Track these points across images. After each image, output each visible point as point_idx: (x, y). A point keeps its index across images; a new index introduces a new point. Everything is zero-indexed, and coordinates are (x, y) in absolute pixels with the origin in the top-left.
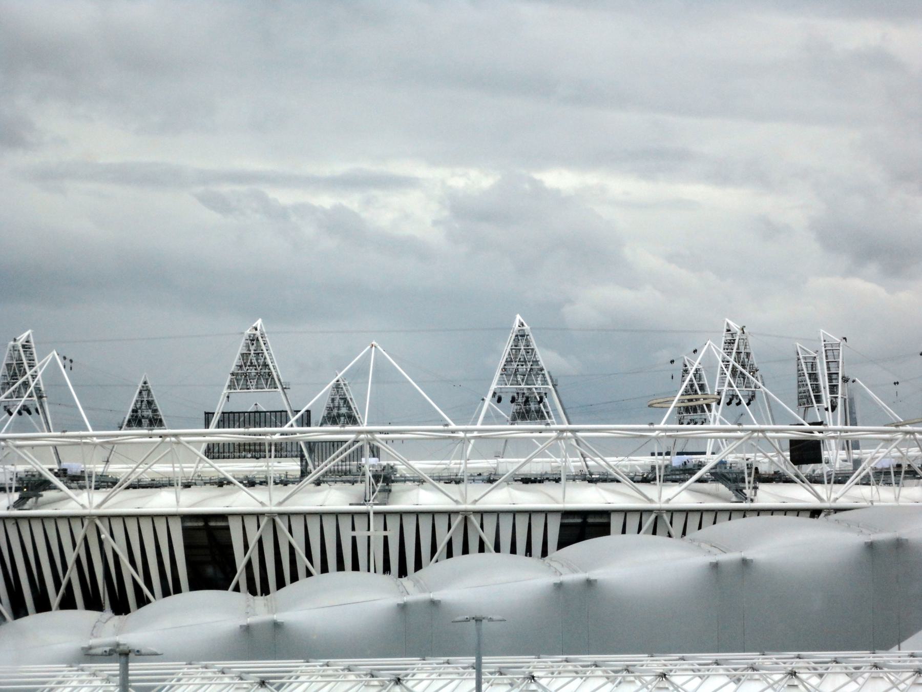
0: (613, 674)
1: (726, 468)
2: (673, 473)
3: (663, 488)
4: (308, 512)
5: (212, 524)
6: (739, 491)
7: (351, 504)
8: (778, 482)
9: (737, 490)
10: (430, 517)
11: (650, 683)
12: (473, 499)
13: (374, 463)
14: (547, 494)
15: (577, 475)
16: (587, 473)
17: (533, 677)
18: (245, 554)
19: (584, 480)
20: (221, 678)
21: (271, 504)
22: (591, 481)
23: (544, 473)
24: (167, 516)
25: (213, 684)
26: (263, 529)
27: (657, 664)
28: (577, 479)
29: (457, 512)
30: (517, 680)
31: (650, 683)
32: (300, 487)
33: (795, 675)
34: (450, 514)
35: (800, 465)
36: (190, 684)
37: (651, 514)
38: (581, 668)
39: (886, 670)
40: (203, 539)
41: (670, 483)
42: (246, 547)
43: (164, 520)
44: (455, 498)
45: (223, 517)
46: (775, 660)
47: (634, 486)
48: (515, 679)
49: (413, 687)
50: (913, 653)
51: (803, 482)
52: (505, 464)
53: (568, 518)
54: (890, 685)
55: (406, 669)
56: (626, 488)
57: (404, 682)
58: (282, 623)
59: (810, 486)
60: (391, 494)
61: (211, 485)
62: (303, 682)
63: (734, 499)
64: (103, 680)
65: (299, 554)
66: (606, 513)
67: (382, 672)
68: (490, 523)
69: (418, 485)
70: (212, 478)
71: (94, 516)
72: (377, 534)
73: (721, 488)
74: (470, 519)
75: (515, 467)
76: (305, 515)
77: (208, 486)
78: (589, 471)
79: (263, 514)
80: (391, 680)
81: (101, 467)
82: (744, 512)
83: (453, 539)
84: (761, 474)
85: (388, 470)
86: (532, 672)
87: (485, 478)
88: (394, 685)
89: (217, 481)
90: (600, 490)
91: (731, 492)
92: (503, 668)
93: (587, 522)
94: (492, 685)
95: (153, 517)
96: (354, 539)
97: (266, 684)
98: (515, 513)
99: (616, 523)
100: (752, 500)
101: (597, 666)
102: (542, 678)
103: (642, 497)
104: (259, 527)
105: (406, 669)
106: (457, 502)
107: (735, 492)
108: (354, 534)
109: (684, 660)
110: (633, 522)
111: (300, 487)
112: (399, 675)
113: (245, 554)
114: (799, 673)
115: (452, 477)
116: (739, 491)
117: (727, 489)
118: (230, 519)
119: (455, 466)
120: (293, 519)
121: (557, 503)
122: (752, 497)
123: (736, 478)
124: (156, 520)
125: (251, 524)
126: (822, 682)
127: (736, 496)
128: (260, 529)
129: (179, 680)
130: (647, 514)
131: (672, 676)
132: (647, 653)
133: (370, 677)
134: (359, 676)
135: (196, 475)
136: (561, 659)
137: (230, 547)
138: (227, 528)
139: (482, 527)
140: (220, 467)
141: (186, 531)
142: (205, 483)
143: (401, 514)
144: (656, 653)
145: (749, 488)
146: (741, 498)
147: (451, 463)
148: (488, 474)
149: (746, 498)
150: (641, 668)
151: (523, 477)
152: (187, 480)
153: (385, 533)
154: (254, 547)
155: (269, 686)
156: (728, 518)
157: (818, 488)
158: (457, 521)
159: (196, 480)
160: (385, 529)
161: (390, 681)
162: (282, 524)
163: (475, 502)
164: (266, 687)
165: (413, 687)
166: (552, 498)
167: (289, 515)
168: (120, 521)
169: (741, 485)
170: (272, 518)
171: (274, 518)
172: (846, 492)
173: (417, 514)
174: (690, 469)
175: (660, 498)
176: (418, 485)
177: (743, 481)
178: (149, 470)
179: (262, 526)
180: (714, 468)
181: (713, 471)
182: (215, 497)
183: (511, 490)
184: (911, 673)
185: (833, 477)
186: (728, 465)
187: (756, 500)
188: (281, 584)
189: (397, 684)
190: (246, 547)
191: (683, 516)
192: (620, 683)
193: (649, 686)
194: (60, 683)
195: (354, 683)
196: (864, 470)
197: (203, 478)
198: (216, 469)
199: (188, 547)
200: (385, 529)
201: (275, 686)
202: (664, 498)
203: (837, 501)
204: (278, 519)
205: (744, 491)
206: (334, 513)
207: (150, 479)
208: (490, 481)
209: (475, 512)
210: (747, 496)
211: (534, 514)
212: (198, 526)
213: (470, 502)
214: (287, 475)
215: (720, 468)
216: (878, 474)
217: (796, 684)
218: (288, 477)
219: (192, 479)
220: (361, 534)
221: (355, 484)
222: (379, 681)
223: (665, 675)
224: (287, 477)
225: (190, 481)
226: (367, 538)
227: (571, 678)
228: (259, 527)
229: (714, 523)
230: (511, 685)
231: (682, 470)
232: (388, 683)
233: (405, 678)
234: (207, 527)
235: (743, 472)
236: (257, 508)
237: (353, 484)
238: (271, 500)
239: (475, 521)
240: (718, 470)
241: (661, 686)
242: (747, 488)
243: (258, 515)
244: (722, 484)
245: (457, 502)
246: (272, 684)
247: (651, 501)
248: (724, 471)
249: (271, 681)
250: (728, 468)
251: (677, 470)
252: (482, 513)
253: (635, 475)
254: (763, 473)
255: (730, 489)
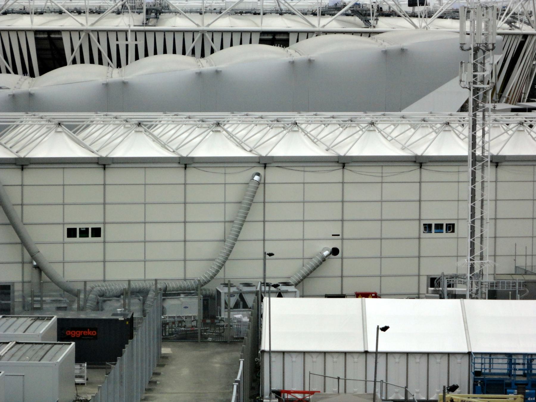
0: (271, 122)
1: (359, 7)
2: (330, 10)
3: (321, 18)
4: (156, 30)
5: (53, 36)
6: (367, 21)
7: (135, 26)
8: (393, 16)
9: (366, 21)
10: (106, 33)
11: (364, 128)
12: (207, 24)
13: (149, 1)
14: (254, 22)
15: (273, 10)
16: (279, 9)
17: (296, 123)
18: (72, 54)
19: (277, 13)
20: (188, 121)
21: (87, 25)
22: (281, 14)
23: (253, 9)
24: (25, 31)
25: (36, 124)
26: (83, 39)
27: (369, 117)
28: (273, 13)
29: (197, 31)
30: (287, 125)
31: (364, 128)
32: (104, 15)
33: (373, 124)
34: (193, 32)
35: (414, 7)
36: (98, 124)
37: (314, 34)
38: (254, 119)
39: (502, 122)
40: (46, 45)
41: (329, 15)
42: (73, 50)
43: (24, 33)
44: (197, 23)
45: (58, 32)
46: (239, 116)
47: (303, 17)
48: (286, 125)
49: (228, 128)
50: (333, 115)
51: (406, 17)
52: (252, 4)
53: (264, 36)
54: (503, 131)
55: (224, 118)
56: (299, 18)
57: (223, 125)
58: (34, 93)
59: (410, 19)
60: (159, 20)
61: (55, 13)
62: (163, 124)
63: (364, 26)
64: (47, 121)
65: (104, 55)
66: (287, 33)
67: (209, 119)
68: (121, 36)
69: (176, 15)
70: (56, 9)
71: (89, 30)
72: (131, 42)
73: (356, 19)
74: (205, 35)
75: (233, 5)
76: (107, 32)
77: (53, 13)
78: (280, 8)
79: (82, 31)
80: (214, 124)
81: (44, 2)
82: (370, 34)
83: (195, 48)
84: (384, 12)
85: (158, 5)
86: (295, 121)
87: (218, 11)
88: (216, 126)
89: (58, 11)
90: (284, 19)
91: (362, 22)
92: (353, 118)
93: (275, 38)
94: (272, 128)
95: (17, 31)
96: (118, 46)
97: (141, 125)
98: (232, 32)
99: (292, 38)
100: (374, 27)
101: (190, 118)
102: (302, 124)
103: (309, 24)
104: (80, 38)
105: (224, 118)
106: (198, 25)
107: (365, 22)
108: (117, 43)
109: (177, 116)
110: (246, 37)
111: (104, 15)
112: (219, 121)
113: (72, 54)
114: (451, 123)
115: (198, 11)
116: (367, 21)
117: (360, 20)
118: (63, 33)
119: (215, 4)
120: (215, 35)
121: (258, 26)
122: (375, 25)
123: (366, 14)
124: (72, 33)
125: (75, 36)
126: (464, 130)
127: (365, 24)
128: (81, 39)
129: (22, 122)
130: (311, 34)
131: (378, 124)
132: (94, 112)
133: (126, 122)
134: (195, 121)
135: (46, 7)
136: (244, 114)
137: (63, 50)
138: (61, 39)
139: (213, 40)
140: (58, 3)
141: (37, 39)
142: (51, 12)
143: (164, 32)
144: (368, 111)
145: (373, 19)
146: (368, 26)
147: (212, 3)
148: (219, 9)
149: (371, 26)
150: (360, 119)
151: (240, 11)
152: (41, 9)
153: (136, 43)
154: (77, 50)
155: (143, 126)
156: (306, 37)
157: (415, 20)
158: (198, 37)
159: (46, 10)
160: (136, 40)
161: (213, 124)
162: (94, 37)
163: (209, 25)
164: (141, 126)
165: (228, 128)
166: (256, 24)
167: (98, 31)
168: (15, 33)
169: (368, 18)
170: (88, 33)
171: (204, 34)
172: (431, 22)
173: (174, 32)
174: (339, 8)
175: (319, 24)
176: (176, 15)
177: (369, 15)
178: (16, 4)
179: (82, 37)
180: (352, 7)
181: (352, 9)
182: (57, 20)
183: (231, 18)
184: (516, 124)
185: (512, 13)
186: (361, 6)
187: (377, 27)
188: (146, 55)
189: (139, 126)
190: (73, 50)
191: (296, 34)
192: (346, 128)
193: (364, 130)
194: (92, 122)
195: (117, 126)
196: (442, 10)
197: (50, 9)
198: (55, 4)
199: (38, 50)
200: (136, 40)
201: (147, 126)
202: (321, 24)
203: (325, 27)
204: (91, 34)
205: (370, 21)
206: (220, 32)
207: (19, 9)
208: (99, 13)
209: (209, 31)
210: (371, 24)
211: (187, 33)
212: (44, 37)
213: (206, 25)
214: (100, 8)
215: (356, 7)
216: (454, 12)
217: (219, 130)
218: (101, 9)
219: (44, 9)
220: (122, 43)
221: (140, 14)
222: (207, 124)
223: (449, 123)
224: (100, 9)
225: (42, 10)
226: (125, 45)
227: (176, 125)
228: (80, 38)
229: (297, 41)
230: (284, 128)
231: (334, 8)
232: (212, 125)
233: (377, 122)
234: (49, 38)
235: (369, 10)
236: (78, 27)
237: (139, 14)
238: (87, 23)
239: (208, 36)
240: (355, 9)
241: (137, 130)
242: (372, 19)
243: (79, 31)
244: (357, 17)
245: (198, 25)
246: (145, 125)
247: (313, 26)
248: (358, 9)
249: (144, 123)
250: (361, 7)
251: (332, 8)
252: (213, 32)
253: (308, 11)
254: (385, 11)
255: (362, 19)
